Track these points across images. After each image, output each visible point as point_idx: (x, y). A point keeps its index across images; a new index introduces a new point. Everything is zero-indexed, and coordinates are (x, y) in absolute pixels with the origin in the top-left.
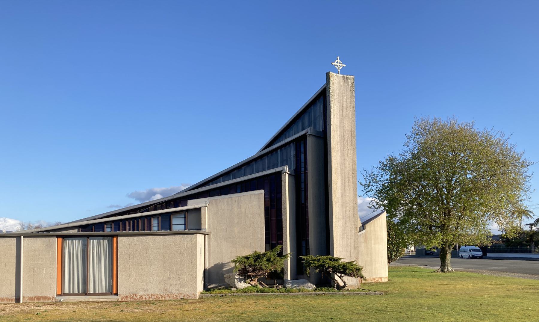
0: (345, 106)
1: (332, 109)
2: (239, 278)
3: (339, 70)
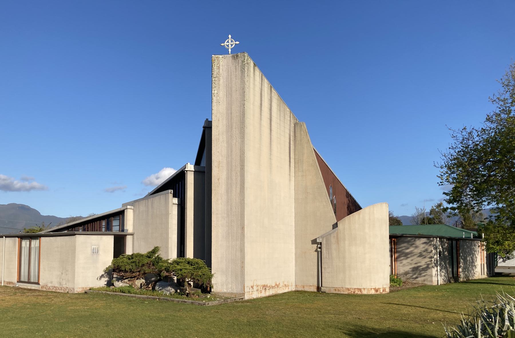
0: (234, 89)
1: (214, 96)
2: (117, 278)
3: (230, 50)
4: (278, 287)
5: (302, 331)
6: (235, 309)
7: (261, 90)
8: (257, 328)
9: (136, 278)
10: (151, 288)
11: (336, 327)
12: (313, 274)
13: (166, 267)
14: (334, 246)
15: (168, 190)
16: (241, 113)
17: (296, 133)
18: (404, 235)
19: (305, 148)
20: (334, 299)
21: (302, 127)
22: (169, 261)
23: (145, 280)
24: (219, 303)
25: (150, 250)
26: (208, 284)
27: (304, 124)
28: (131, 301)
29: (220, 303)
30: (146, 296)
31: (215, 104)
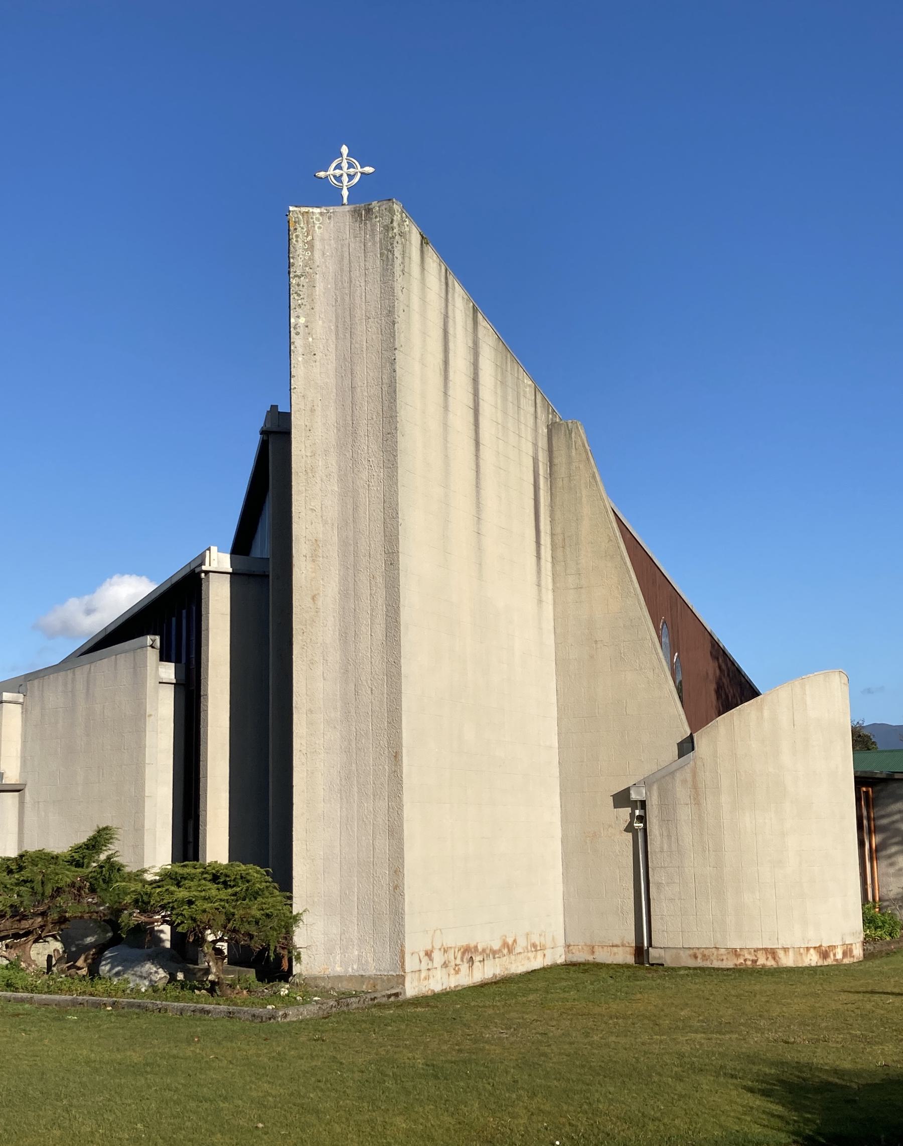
0: (359, 313)
3: (345, 193)
4: (510, 951)
5: (612, 1089)
6: (379, 1026)
7: (446, 317)
8: (462, 1084)
9: (31, 938)
10: (84, 972)
11: (720, 1071)
12: (622, 908)
13: (139, 897)
14: (684, 813)
15: (141, 638)
16: (385, 388)
17: (556, 453)
18: (897, 776)
19: (584, 499)
20: (696, 984)
21: (573, 435)
22: (149, 877)
23: (62, 942)
24: (321, 1013)
25: (83, 839)
26: (283, 948)
27: (578, 428)
28: (18, 1015)
29: (324, 1010)
30: (68, 997)
31: (300, 359)
